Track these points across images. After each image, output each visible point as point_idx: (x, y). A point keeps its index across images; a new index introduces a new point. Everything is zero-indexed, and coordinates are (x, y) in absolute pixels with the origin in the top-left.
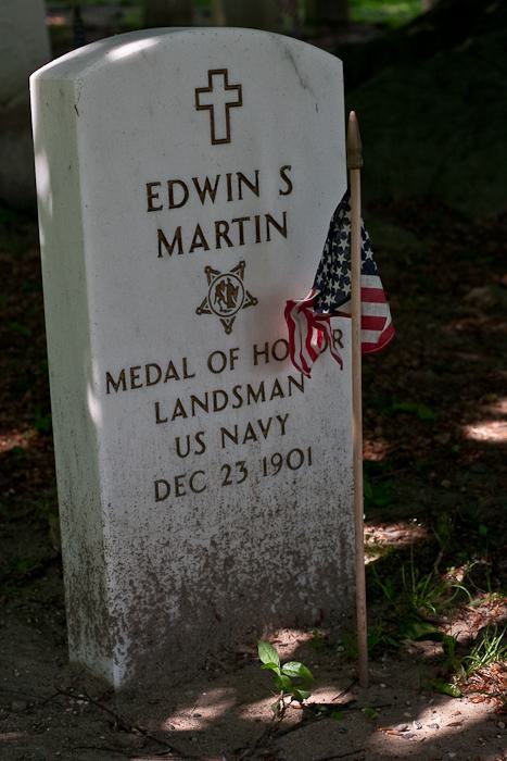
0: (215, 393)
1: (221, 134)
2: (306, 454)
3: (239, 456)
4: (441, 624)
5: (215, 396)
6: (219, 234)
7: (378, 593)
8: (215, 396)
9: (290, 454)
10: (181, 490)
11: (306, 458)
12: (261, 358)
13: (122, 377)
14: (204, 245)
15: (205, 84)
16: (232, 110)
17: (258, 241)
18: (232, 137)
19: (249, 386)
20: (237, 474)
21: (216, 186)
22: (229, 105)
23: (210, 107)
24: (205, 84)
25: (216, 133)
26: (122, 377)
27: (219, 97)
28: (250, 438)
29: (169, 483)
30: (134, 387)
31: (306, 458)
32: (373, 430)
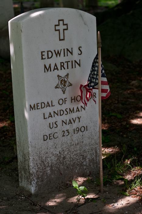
0: (60, 111)
1: (62, 38)
2: (86, 128)
3: (67, 128)
4: (124, 175)
5: (60, 111)
6: (61, 66)
7: (106, 167)
8: (60, 111)
9: (81, 128)
10: (51, 138)
11: (86, 129)
12: (73, 101)
13: (34, 106)
14: (57, 69)
15: (58, 24)
16: (65, 31)
17: (72, 68)
18: (65, 39)
19: (70, 108)
20: (66, 133)
21: (61, 52)
22: (64, 30)
23: (59, 30)
24: (58, 24)
25: (60, 37)
26: (34, 106)
27: (61, 27)
28: (70, 123)
29: (47, 136)
30: (37, 109)
31: (86, 129)
32: (104, 121)
